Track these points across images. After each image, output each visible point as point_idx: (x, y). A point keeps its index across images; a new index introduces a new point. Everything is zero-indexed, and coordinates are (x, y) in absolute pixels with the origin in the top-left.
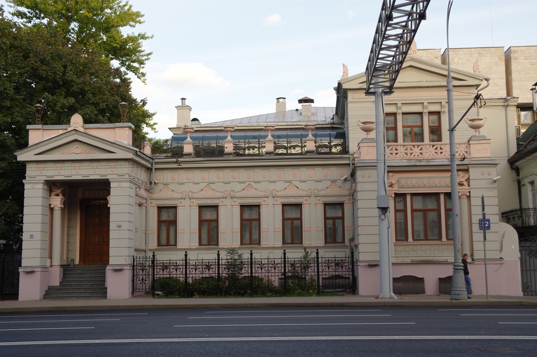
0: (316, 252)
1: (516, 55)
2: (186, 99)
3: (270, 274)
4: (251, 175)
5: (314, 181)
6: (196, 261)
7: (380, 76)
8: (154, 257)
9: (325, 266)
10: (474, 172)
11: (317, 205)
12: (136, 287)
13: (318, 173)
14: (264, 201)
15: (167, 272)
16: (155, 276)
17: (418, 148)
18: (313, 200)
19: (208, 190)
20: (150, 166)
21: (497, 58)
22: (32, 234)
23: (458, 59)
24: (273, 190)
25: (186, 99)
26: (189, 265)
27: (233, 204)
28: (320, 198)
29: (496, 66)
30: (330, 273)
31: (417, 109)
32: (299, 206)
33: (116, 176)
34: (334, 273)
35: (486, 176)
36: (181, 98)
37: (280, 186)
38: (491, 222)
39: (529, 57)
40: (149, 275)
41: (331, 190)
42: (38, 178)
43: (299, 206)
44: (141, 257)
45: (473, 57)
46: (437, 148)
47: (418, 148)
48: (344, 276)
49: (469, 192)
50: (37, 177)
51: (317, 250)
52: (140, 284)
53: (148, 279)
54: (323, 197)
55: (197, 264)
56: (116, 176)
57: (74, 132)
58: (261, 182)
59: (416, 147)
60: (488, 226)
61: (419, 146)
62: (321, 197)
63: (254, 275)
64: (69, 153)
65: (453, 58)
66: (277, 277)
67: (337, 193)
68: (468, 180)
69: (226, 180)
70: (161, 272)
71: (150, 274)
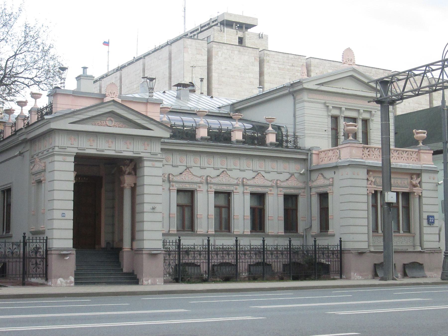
0: (23, 236)
1: (268, 58)
2: (88, 68)
3: (7, 260)
4: (224, 162)
5: (288, 173)
6: (200, 246)
7: (390, 86)
8: (180, 242)
9: (197, 254)
10: (425, 177)
11: (279, 195)
12: (29, 272)
13: (280, 166)
14: (271, 190)
15: (191, 257)
16: (181, 261)
17: (396, 152)
18: (274, 191)
19: (260, 178)
20: (304, 157)
21: (253, 58)
22: (64, 212)
23: (222, 54)
24: (169, 174)
25: (88, 68)
26: (266, 251)
27: (279, 193)
28: (281, 189)
29: (252, 66)
30: (219, 261)
31: (353, 114)
32: (228, 194)
33: (149, 155)
34: (222, 261)
35: (432, 181)
36: (82, 67)
37: (249, 175)
38: (435, 218)
39: (278, 62)
40: (176, 260)
41: (291, 182)
42: (69, 150)
43: (228, 194)
44: (171, 241)
45: (234, 54)
46: (399, 153)
47: (396, 152)
48: (268, 263)
49: (421, 193)
50: (105, 151)
51: (209, 238)
52: (167, 269)
53: (42, 263)
54: (250, 187)
55: (201, 250)
56: (149, 155)
57: (112, 103)
58: (179, 166)
59: (366, 149)
60: (433, 221)
61: (407, 151)
62: (175, 183)
63: (265, 261)
64: (102, 125)
65: (218, 51)
66: (246, 264)
67: (296, 185)
68: (420, 183)
69: (279, 171)
70: (227, 257)
71: (177, 259)
